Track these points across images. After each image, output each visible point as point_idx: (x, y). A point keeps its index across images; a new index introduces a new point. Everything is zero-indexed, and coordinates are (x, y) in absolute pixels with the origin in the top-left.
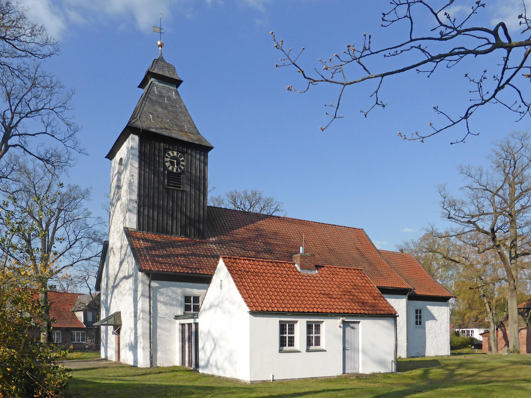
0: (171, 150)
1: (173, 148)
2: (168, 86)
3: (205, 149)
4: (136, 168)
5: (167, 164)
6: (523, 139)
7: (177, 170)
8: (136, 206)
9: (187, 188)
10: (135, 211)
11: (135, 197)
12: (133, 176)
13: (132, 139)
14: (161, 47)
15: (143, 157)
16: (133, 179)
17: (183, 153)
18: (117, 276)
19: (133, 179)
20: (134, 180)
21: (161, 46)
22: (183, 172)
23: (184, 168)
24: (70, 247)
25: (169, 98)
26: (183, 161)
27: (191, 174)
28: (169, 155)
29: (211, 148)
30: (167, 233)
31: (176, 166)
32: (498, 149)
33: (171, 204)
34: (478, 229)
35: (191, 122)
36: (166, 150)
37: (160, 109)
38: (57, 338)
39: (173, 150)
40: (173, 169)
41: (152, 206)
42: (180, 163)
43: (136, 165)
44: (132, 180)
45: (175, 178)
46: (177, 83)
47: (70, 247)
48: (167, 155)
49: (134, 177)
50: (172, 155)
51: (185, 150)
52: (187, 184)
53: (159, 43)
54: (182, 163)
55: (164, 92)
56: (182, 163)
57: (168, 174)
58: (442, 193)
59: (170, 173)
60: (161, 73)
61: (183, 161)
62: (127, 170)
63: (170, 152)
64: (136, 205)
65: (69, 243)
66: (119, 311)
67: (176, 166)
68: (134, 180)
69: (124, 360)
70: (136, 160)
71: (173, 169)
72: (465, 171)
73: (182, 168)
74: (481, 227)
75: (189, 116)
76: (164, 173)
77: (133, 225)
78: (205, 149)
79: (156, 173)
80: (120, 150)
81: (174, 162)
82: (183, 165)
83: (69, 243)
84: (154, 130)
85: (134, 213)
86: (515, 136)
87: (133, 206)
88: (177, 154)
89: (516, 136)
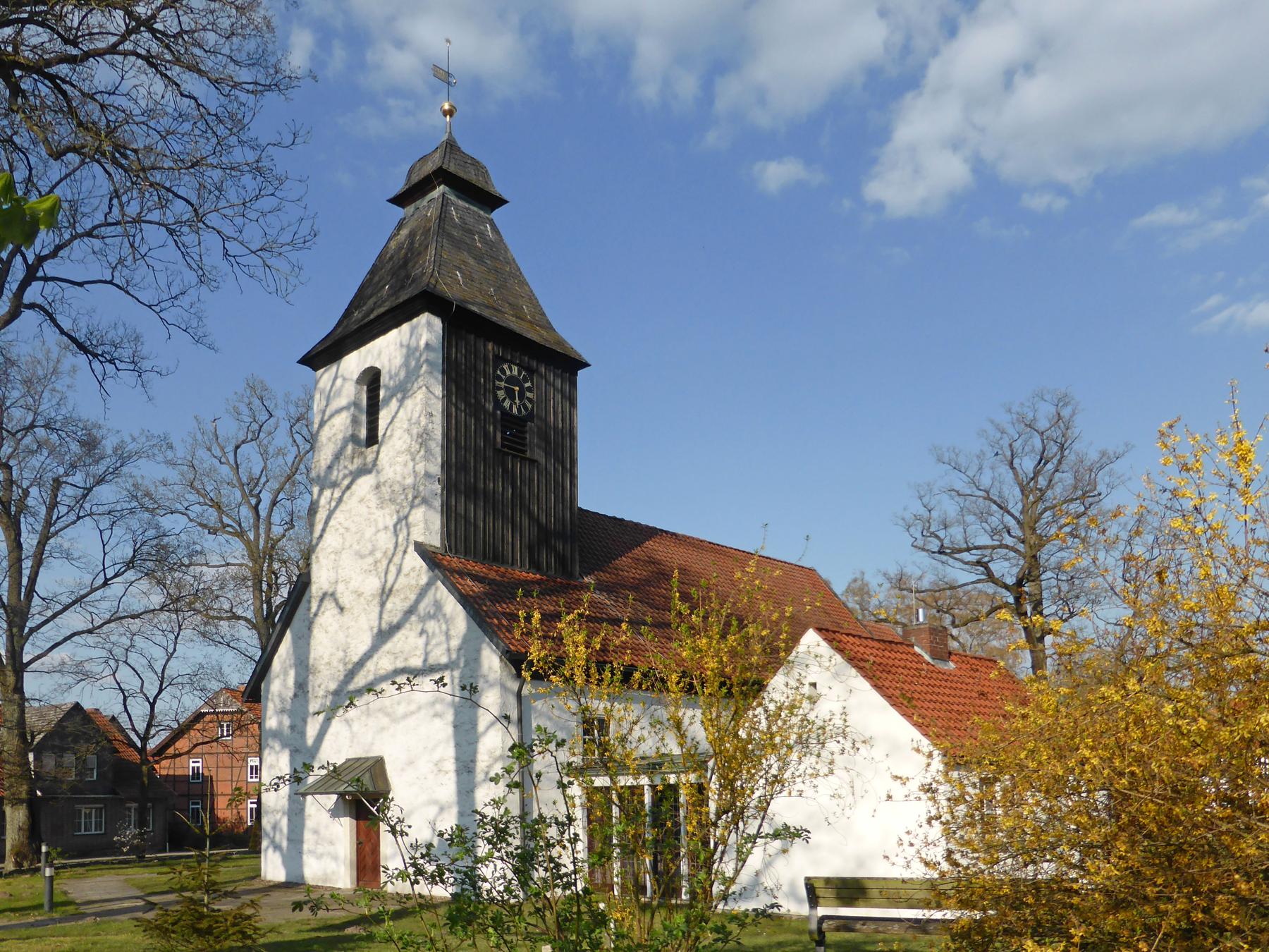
0: (506, 361)
1: (512, 356)
2: (475, 209)
3: (570, 365)
4: (437, 397)
5: (501, 394)
6: (1061, 404)
7: (519, 410)
8: (439, 491)
9: (540, 456)
10: (437, 503)
11: (435, 468)
12: (431, 415)
13: (429, 324)
14: (451, 116)
15: (454, 375)
16: (432, 422)
17: (531, 372)
18: (361, 664)
19: (432, 422)
20: (435, 426)
21: (450, 113)
22: (530, 416)
23: (533, 407)
24: (105, 584)
25: (482, 235)
26: (529, 389)
27: (546, 421)
28: (503, 372)
29: (585, 365)
30: (504, 562)
31: (517, 401)
32: (1004, 419)
33: (510, 491)
34: (990, 577)
35: (532, 299)
36: (499, 360)
37: (471, 261)
38: (91, 818)
39: (511, 362)
40: (511, 407)
41: (472, 493)
42: (524, 394)
43: (438, 390)
44: (430, 426)
45: (514, 425)
46: (493, 202)
47: (105, 584)
48: (499, 372)
49: (434, 418)
50: (508, 373)
51: (535, 364)
52: (539, 447)
53: (446, 107)
54: (528, 394)
55: (470, 220)
56: (528, 394)
57: (502, 419)
58: (926, 500)
59: (507, 415)
60: (461, 174)
61: (529, 389)
62: (409, 403)
63: (505, 367)
64: (438, 488)
65: (104, 569)
66: (374, 753)
67: (517, 401)
68: (435, 426)
69: (313, 879)
70: (436, 379)
71: (511, 407)
72: (946, 460)
73: (529, 406)
74: (997, 575)
75: (527, 284)
76: (494, 414)
77: (434, 540)
78: (570, 365)
79: (476, 410)
80: (363, 349)
81: (514, 391)
82: (530, 400)
83: (104, 569)
84: (474, 308)
85: (435, 508)
86: (1045, 398)
87: (432, 491)
88: (520, 373)
89: (1047, 397)
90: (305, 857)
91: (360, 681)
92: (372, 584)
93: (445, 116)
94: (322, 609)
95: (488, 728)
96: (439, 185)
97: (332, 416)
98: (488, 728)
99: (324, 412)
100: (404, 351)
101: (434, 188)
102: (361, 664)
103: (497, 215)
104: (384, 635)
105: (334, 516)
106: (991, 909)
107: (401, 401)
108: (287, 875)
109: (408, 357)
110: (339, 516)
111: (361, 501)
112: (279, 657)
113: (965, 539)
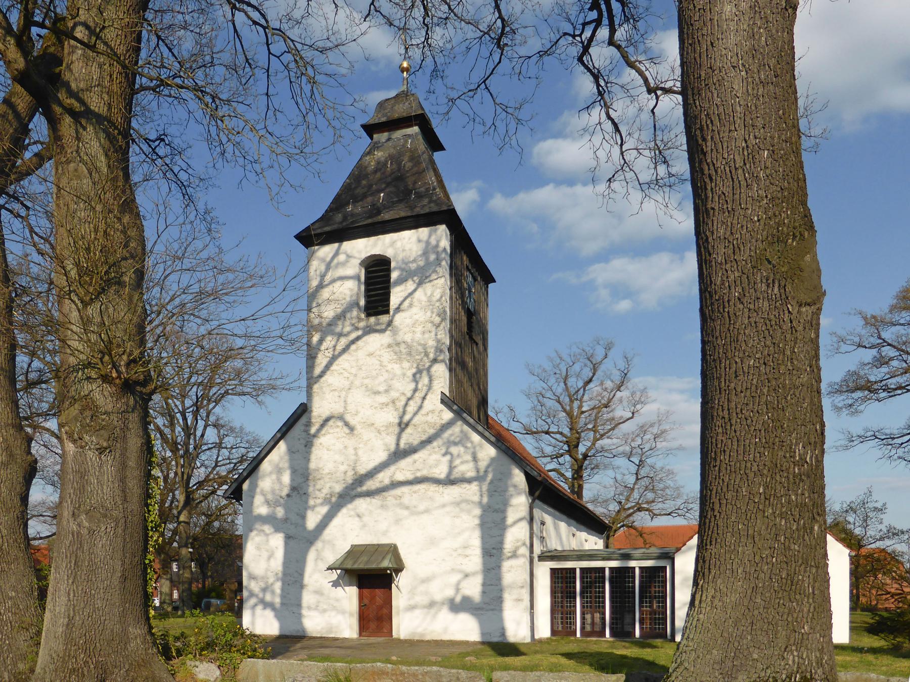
90: (304, 612)
91: (371, 485)
92: (391, 417)
93: (403, 72)
94: (323, 432)
95: (515, 523)
96: (416, 125)
97: (334, 281)
98: (515, 523)
99: (323, 276)
100: (423, 245)
101: (411, 126)
102: (371, 474)
103: (437, 156)
104: (398, 454)
105: (337, 362)
106: (171, 568)
107: (420, 284)
108: (281, 628)
109: (425, 253)
110: (343, 362)
111: (370, 355)
112: (270, 461)
113: (554, 394)
